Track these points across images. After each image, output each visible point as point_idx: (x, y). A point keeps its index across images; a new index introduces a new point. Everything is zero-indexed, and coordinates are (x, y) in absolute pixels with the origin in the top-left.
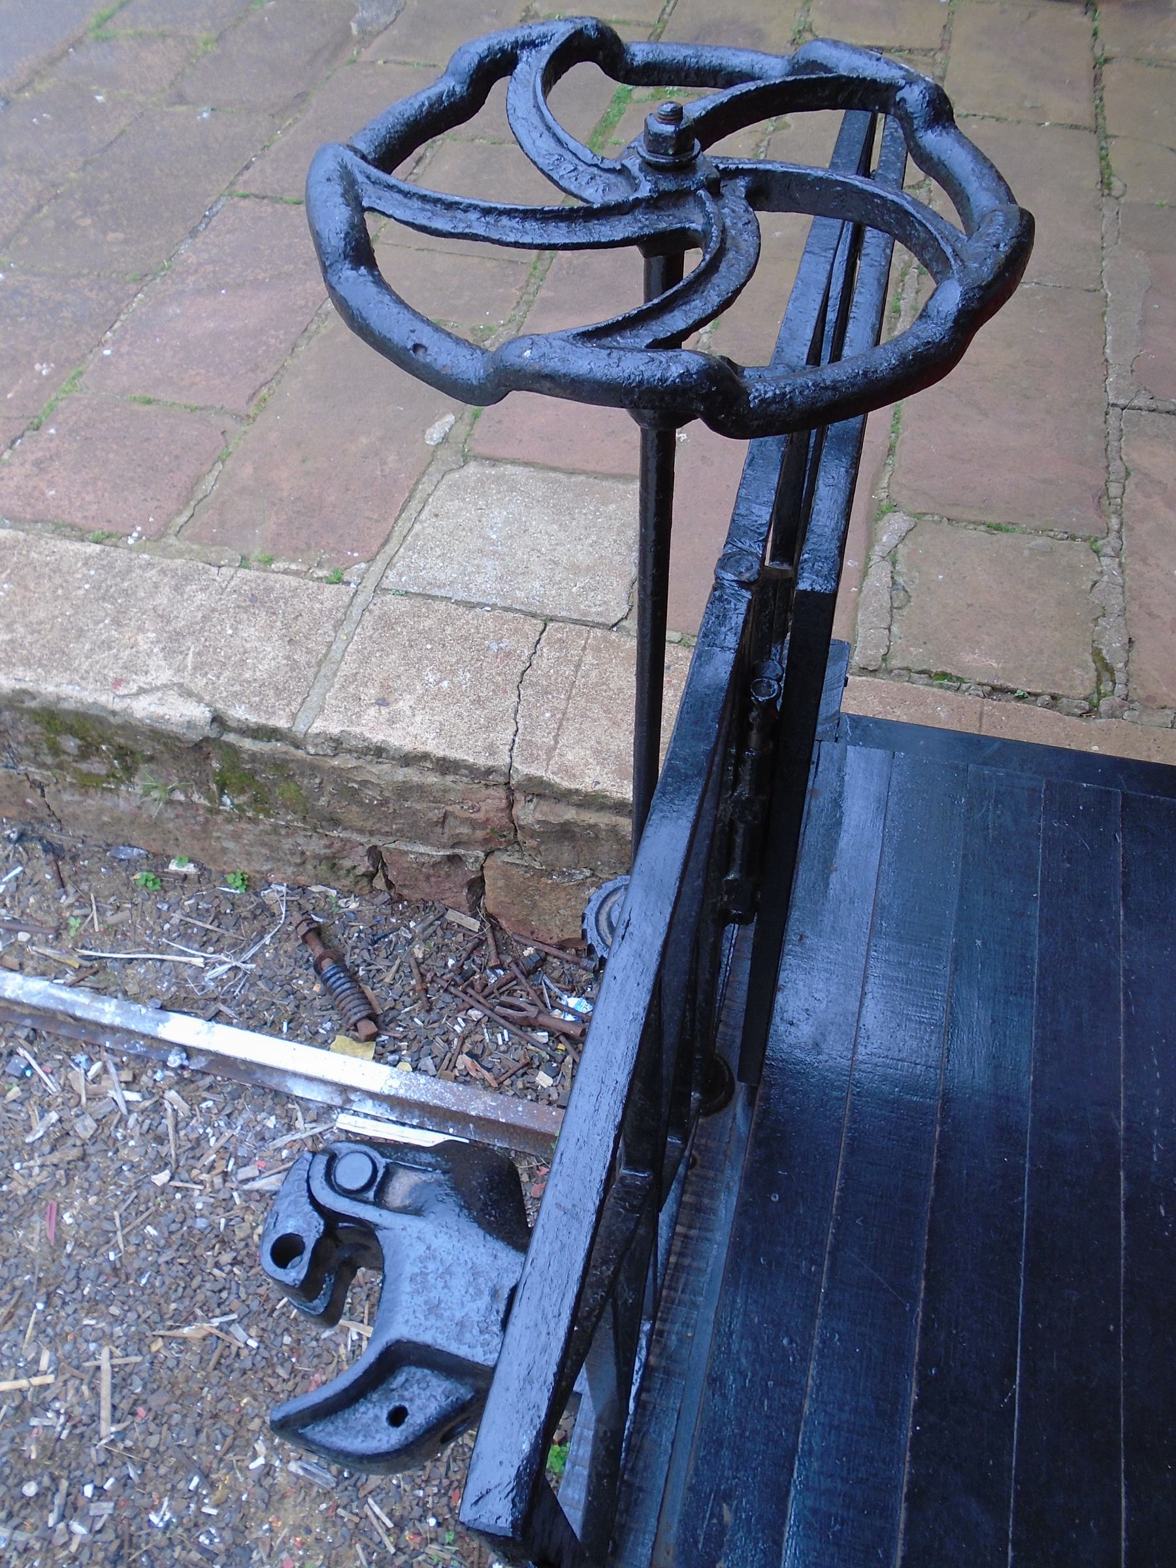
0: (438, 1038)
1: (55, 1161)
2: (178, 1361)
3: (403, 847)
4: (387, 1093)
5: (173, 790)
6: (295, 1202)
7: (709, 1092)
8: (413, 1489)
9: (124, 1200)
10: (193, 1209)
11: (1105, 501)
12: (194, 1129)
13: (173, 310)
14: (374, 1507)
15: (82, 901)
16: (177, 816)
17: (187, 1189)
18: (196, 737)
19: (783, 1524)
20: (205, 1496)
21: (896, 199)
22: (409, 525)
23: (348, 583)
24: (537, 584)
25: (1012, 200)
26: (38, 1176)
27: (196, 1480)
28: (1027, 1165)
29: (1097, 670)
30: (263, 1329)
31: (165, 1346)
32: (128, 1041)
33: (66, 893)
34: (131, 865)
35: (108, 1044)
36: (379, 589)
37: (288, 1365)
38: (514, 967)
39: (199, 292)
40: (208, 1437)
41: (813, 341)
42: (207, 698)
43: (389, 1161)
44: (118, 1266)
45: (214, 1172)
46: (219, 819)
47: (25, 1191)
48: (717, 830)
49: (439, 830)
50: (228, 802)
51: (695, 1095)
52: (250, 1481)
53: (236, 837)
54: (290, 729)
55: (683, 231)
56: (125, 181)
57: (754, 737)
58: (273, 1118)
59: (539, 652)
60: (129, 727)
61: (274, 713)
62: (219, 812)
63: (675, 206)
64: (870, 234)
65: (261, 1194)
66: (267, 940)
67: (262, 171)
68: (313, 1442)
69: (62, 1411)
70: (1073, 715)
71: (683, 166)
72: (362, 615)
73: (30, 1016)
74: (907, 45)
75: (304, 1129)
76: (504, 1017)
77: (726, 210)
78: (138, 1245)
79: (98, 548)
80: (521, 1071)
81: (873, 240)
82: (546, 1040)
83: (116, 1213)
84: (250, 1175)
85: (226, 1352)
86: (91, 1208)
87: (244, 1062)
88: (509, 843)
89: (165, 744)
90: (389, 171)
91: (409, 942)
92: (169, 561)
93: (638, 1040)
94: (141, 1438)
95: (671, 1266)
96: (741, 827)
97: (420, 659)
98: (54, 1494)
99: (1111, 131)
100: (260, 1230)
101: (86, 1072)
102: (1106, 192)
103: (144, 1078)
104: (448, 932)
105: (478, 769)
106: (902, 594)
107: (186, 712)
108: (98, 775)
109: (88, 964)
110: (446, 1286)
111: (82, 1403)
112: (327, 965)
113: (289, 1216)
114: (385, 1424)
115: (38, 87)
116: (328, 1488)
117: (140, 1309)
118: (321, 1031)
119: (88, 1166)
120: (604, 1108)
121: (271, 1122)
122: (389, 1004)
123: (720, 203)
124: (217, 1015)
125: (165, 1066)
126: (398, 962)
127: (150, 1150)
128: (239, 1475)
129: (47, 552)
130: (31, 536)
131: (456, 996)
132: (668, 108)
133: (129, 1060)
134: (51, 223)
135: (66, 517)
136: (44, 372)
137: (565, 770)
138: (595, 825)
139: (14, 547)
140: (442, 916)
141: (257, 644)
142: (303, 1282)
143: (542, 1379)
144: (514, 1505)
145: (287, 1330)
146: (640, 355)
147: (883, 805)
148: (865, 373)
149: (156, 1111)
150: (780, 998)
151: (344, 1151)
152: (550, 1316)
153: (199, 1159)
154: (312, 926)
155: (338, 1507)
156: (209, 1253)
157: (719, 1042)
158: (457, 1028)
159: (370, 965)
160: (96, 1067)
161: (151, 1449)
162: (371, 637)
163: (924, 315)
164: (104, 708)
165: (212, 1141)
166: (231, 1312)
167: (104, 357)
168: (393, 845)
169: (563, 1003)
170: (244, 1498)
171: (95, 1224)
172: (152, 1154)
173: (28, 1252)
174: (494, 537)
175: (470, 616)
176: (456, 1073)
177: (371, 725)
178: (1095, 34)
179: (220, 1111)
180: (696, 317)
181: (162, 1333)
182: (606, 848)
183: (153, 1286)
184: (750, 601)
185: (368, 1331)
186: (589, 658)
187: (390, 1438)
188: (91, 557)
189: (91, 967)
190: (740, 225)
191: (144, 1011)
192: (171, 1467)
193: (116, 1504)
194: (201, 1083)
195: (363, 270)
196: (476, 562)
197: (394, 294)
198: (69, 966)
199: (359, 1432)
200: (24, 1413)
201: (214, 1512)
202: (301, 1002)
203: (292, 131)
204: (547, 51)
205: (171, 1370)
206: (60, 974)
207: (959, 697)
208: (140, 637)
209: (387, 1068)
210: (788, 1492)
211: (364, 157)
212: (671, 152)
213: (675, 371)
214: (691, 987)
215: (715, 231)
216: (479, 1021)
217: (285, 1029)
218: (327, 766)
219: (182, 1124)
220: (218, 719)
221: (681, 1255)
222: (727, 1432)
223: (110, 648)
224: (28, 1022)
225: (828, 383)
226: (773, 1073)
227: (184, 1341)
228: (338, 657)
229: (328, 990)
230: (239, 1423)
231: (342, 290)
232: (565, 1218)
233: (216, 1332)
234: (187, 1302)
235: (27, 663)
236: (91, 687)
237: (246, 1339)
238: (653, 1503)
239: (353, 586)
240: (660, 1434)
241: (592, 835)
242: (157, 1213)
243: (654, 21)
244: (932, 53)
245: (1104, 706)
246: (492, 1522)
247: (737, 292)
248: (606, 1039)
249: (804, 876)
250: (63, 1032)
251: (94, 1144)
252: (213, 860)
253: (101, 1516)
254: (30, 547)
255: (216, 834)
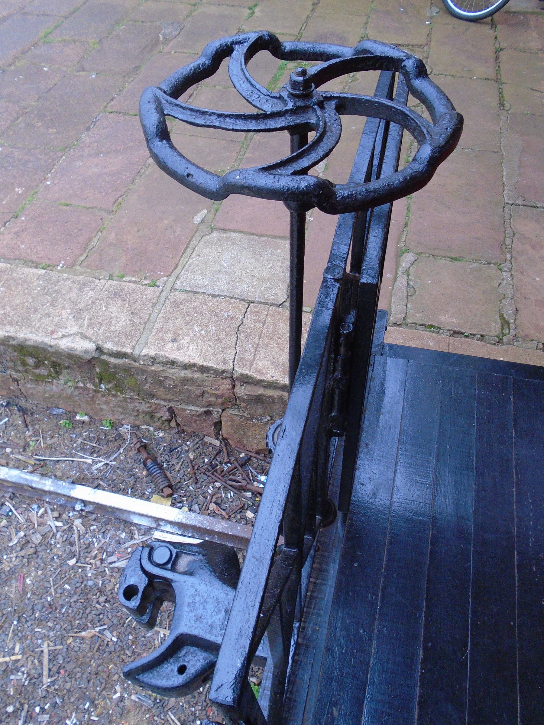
0: (200, 496)
1: (23, 554)
2: (80, 648)
3: (184, 407)
4: (177, 521)
5: (78, 382)
6: (134, 570)
7: (325, 516)
8: (189, 707)
9: (55, 573)
10: (86, 576)
11: (504, 247)
12: (87, 539)
13: (79, 163)
14: (171, 716)
15: (36, 434)
16: (80, 394)
17: (84, 567)
18: (89, 357)
19: (361, 716)
20: (92, 712)
21: (402, 109)
22: (186, 260)
23: (158, 286)
24: (245, 286)
25: (454, 109)
26: (15, 562)
27: (88, 704)
28: (472, 549)
29: (501, 323)
30: (120, 633)
31: (74, 641)
32: (57, 498)
33: (28, 430)
34: (58, 417)
35: (47, 500)
36: (173, 289)
37: (131, 649)
38: (235, 462)
39: (90, 155)
40: (93, 683)
41: (367, 173)
42: (94, 339)
43: (178, 550)
44: (52, 603)
45: (97, 559)
46: (99, 395)
47: (9, 569)
48: (326, 392)
49: (200, 399)
50: (103, 387)
51: (318, 517)
52: (113, 704)
53: (107, 403)
54: (132, 353)
55: (307, 124)
56: (57, 106)
57: (342, 349)
58: (124, 534)
59: (246, 317)
60: (58, 353)
61: (125, 346)
62: (99, 392)
63: (304, 112)
64: (392, 125)
65: (118, 569)
66: (121, 451)
67: (120, 101)
68: (143, 682)
69: (25, 672)
70: (491, 344)
71: (307, 95)
72: (165, 301)
73: (11, 487)
74: (412, 43)
75: (139, 539)
76: (231, 486)
77: (326, 114)
78: (61, 593)
79: (44, 271)
80: (239, 511)
81: (393, 128)
82: (250, 496)
83: (51, 579)
84: (113, 560)
85: (102, 644)
86: (39, 577)
87: (111, 507)
88: (233, 405)
89: (74, 361)
90: (176, 98)
91: (187, 451)
92: (76, 277)
93: (289, 483)
94: (62, 684)
95: (308, 597)
96: (337, 391)
97: (191, 321)
98: (21, 711)
99: (503, 80)
100: (118, 586)
101: (37, 513)
102: (502, 108)
103: (64, 516)
104: (205, 447)
105: (219, 371)
106: (412, 289)
107: (84, 346)
108: (43, 375)
109: (38, 463)
110: (204, 608)
111: (35, 668)
112: (149, 462)
113: (131, 576)
114: (176, 673)
115: (17, 64)
116: (150, 707)
117: (62, 623)
118: (147, 493)
119: (37, 557)
120: (274, 513)
121: (123, 535)
122: (178, 480)
123: (324, 111)
124: (98, 486)
125: (74, 510)
126: (182, 460)
127: (67, 549)
128: (108, 701)
129: (20, 273)
130: (13, 266)
131: (209, 476)
132: (300, 70)
133: (57, 507)
134: (23, 125)
135: (30, 258)
136: (20, 192)
137: (259, 371)
138: (272, 396)
139: (5, 271)
140: (202, 439)
141: (117, 314)
142: (138, 607)
143: (246, 635)
144: (234, 691)
145: (130, 633)
146: (288, 178)
147: (404, 385)
148: (388, 185)
149: (70, 531)
150: (357, 473)
151: (157, 546)
152: (250, 606)
153: (89, 553)
154: (142, 444)
155: (154, 716)
156: (94, 597)
157: (329, 493)
158: (209, 491)
159: (169, 462)
160: (42, 511)
161: (67, 690)
162: (169, 311)
163: (415, 159)
164: (46, 344)
165: (96, 544)
166: (105, 624)
167: (47, 185)
168: (179, 406)
169: (258, 479)
170: (110, 712)
171: (41, 584)
172: (68, 551)
173: (10, 597)
174: (225, 265)
175: (215, 301)
176: (209, 512)
177: (169, 351)
178: (496, 38)
179: (99, 531)
180: (313, 161)
181: (72, 635)
182: (277, 407)
183: (68, 613)
184: (339, 288)
185: (167, 633)
186: (269, 320)
187: (178, 680)
188: (41, 275)
189: (40, 464)
190: (332, 121)
191: (64, 484)
192: (76, 698)
193: (50, 716)
194: (90, 518)
195: (164, 142)
196: (217, 276)
197: (179, 152)
198: (30, 464)
199: (164, 677)
200: (7, 673)
201: (96, 719)
202: (137, 479)
203: (133, 83)
204: (246, 46)
205: (76, 652)
206: (25, 467)
207: (439, 336)
208: (63, 312)
209: (177, 510)
210: (363, 702)
211: (165, 92)
212: (301, 89)
213: (304, 184)
214: (315, 463)
215: (321, 123)
216: (220, 487)
217: (130, 492)
218: (149, 370)
219: (82, 537)
220: (99, 349)
221: (313, 591)
222: (335, 674)
223: (49, 317)
224: (10, 490)
225: (372, 189)
226: (354, 507)
227: (83, 638)
228: (154, 320)
229: (150, 474)
230: (108, 677)
231: (155, 151)
232: (257, 562)
233: (98, 634)
234: (84, 620)
235: (11, 324)
236: (40, 334)
237: (111, 637)
238: (300, 708)
239: (160, 287)
240: (304, 675)
241: (271, 400)
242: (70, 579)
243: (296, 33)
244: (422, 47)
245: (505, 340)
246: (224, 699)
247: (331, 150)
248: (275, 482)
249: (368, 416)
250: (27, 494)
251: (41, 546)
252: (96, 414)
253: (43, 722)
254: (13, 271)
255: (97, 402)
